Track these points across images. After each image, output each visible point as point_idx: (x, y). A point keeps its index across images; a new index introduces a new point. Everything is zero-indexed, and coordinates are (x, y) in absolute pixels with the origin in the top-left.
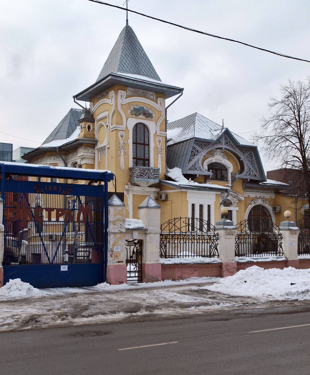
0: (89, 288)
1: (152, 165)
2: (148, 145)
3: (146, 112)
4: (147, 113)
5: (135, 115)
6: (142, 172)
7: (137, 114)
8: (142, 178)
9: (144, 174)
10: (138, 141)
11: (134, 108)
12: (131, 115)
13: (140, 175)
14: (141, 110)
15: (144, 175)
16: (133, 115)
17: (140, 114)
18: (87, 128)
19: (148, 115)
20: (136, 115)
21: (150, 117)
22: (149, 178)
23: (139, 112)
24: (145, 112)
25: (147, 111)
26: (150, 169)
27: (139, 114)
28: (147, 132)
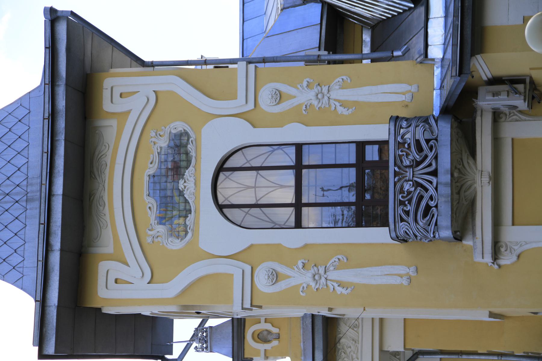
1: (381, 132)
2: (299, 147)
4: (170, 159)
5: (186, 217)
6: (410, 208)
8: (436, 206)
9: (421, 198)
10: (289, 197)
11: (162, 220)
13: (425, 215)
15: (426, 196)
16: (185, 225)
17: (181, 194)
18: (267, 346)
19: (178, 158)
20: (185, 209)
21: (186, 146)
22: (435, 173)
23: (172, 197)
24: (168, 169)
25: (166, 161)
26: (397, 169)
27: (181, 198)
28: (250, 153)
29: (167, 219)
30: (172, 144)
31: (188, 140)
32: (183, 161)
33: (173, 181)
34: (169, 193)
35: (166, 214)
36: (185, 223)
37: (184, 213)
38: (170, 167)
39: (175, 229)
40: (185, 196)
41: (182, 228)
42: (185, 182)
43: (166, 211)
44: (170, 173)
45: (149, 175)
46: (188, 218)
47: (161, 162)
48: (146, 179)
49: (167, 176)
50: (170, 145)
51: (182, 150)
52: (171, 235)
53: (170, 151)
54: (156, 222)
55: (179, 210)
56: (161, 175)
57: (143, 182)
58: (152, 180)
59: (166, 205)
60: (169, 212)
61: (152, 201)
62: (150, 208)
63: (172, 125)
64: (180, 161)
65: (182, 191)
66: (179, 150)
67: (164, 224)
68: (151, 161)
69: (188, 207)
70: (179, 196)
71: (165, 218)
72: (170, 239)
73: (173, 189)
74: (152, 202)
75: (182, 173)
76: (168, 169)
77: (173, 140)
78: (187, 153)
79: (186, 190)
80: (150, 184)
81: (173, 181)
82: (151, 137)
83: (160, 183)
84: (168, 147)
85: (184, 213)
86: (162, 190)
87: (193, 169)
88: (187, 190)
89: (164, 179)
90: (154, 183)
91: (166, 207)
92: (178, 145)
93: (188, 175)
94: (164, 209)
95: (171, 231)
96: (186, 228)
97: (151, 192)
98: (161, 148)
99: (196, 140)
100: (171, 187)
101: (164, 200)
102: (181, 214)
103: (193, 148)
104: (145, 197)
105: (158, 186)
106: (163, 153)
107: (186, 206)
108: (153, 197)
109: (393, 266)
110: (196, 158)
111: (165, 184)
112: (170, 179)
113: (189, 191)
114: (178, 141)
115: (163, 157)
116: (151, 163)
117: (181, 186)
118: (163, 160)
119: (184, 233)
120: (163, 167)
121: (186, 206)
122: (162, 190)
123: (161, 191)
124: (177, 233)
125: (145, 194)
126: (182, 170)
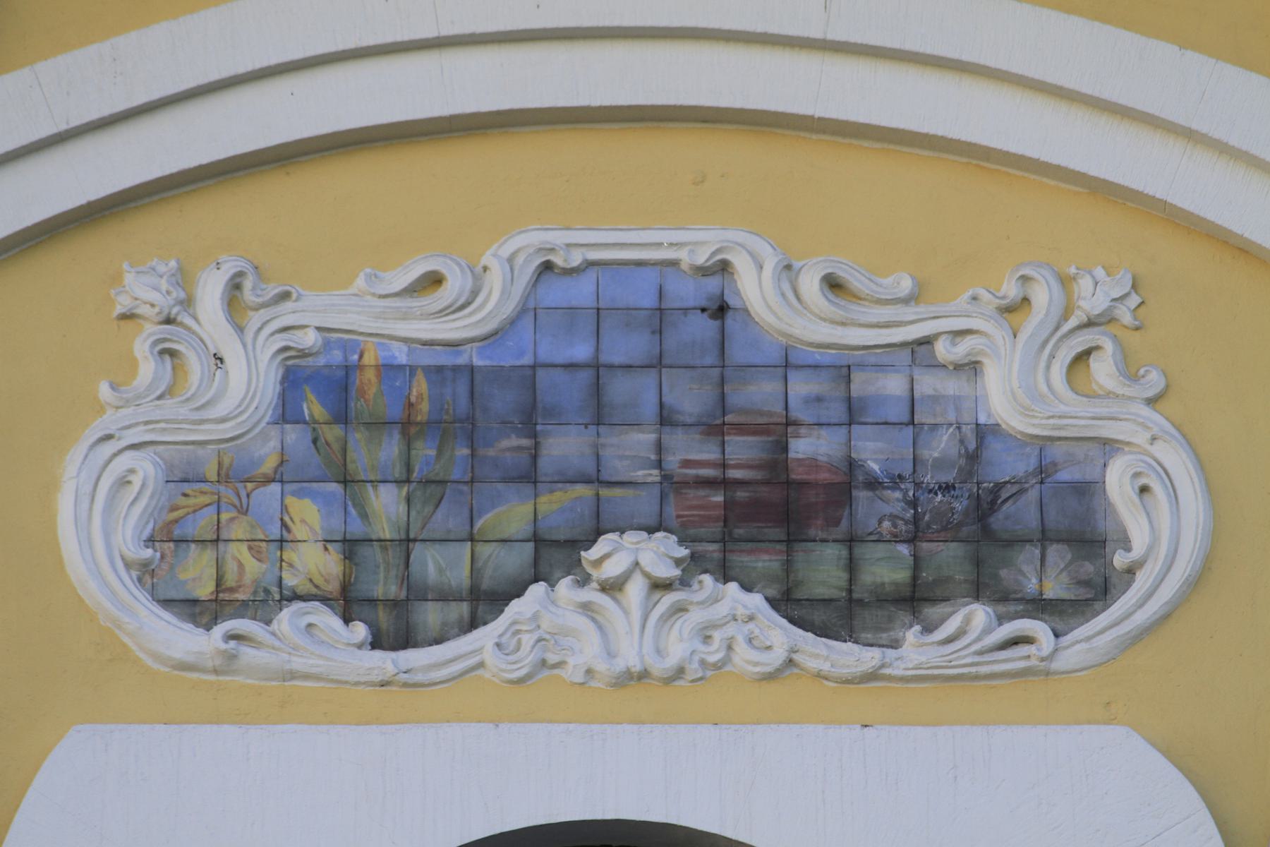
0: (109, 624)
3: (802, 447)
4: (874, 452)
5: (348, 603)
7: (441, 564)
11: (324, 388)
12: (200, 643)
14: (599, 414)
16: (269, 600)
17: (555, 554)
20: (416, 593)
21: (983, 587)
23: (528, 476)
24: (780, 430)
25: (854, 413)
27: (517, 559)
29: (332, 433)
30: (1006, 465)
31: (1040, 607)
32: (852, 566)
33: (671, 484)
34: (565, 446)
35: (377, 425)
36: (296, 597)
37: (384, 586)
38: (802, 447)
39: (243, 511)
40: (537, 590)
41: (248, 566)
42: (660, 586)
43: (408, 427)
44: (743, 451)
45: (724, 268)
46: (328, 620)
47: (844, 373)
48: (694, 244)
49: (715, 429)
50: (994, 448)
51: (947, 556)
52: (183, 477)
53: (942, 445)
54: (309, 339)
55: (407, 542)
56: (723, 370)
57: (660, 225)
58: (687, 292)
59: (467, 427)
60: (390, 449)
61: (497, 301)
62: (434, 280)
63: (1175, 459)
64: (851, 541)
65: (573, 566)
66: (949, 529)
67: (287, 413)
68: (856, 281)
69: (430, 615)
70: (537, 540)
71: (342, 417)
72: (145, 468)
73: (596, 479)
74: (476, 303)
75: (740, 559)
76: (780, 430)
77: (1043, 472)
78: (916, 599)
79: (590, 594)
80: (652, 276)
81: (671, 484)
82: (1066, 282)
83: (658, 363)
84: (984, 433)
85: (384, 586)
86: (597, 390)
87: (776, 657)
88: (586, 608)
89: (690, 398)
90: (660, 317)
91: (442, 428)
92: (997, 522)
93: (722, 609)
94: (424, 410)
95: (224, 476)
96: (243, 609)
97: (582, 292)
98: (971, 368)
99: (1041, 673)
100: (617, 467)
101: (503, 401)
102: (372, 554)
103: (962, 657)
104: (527, 242)
105: (626, 346)
106: (927, 383)
107: (445, 596)
108: (528, 311)
109: (398, 727)
110: (872, 676)
111: (649, 409)
112: (690, 450)
113: (581, 622)
114: (1031, 519)
115: (894, 385)
116: (833, 284)
117: (614, 554)
118: (861, 384)
119: (205, 591)
120: (800, 387)
121: (445, 596)
122: (597, 390)
123: (585, 376)
124: (202, 525)
125: (558, 238)
126: (766, 562)
